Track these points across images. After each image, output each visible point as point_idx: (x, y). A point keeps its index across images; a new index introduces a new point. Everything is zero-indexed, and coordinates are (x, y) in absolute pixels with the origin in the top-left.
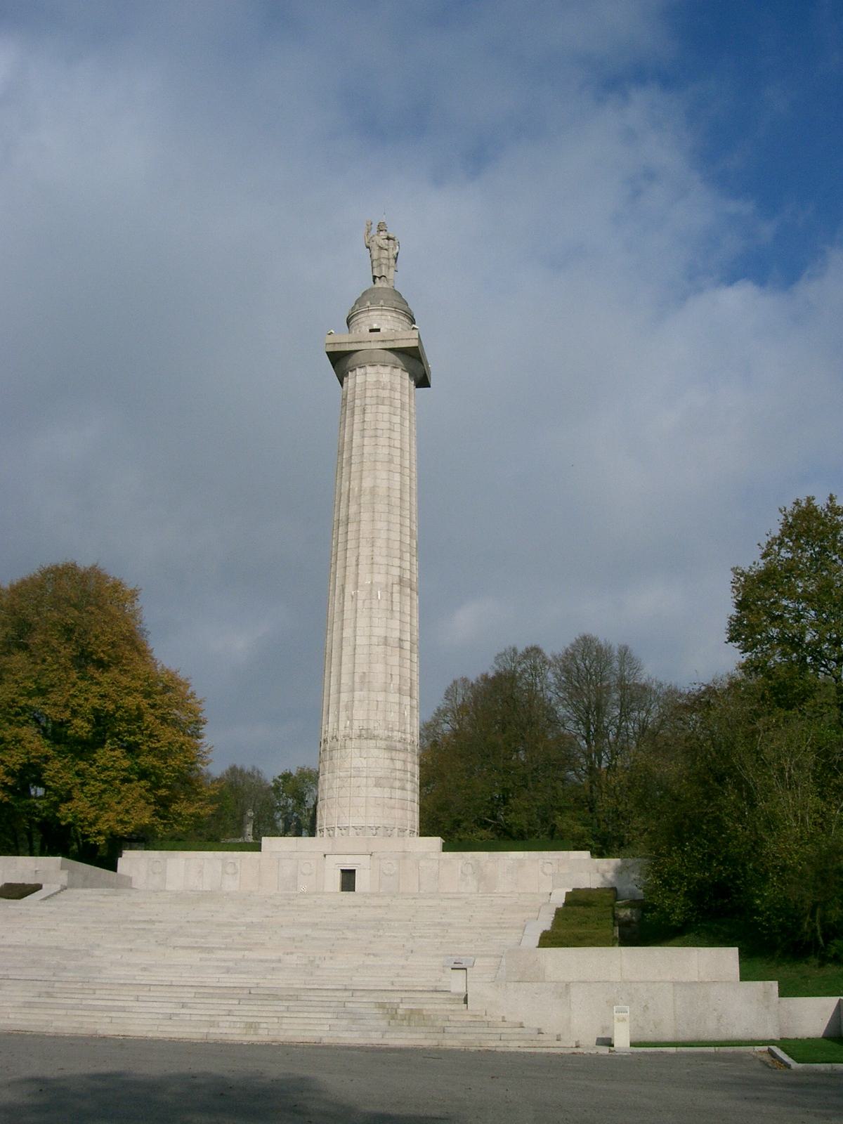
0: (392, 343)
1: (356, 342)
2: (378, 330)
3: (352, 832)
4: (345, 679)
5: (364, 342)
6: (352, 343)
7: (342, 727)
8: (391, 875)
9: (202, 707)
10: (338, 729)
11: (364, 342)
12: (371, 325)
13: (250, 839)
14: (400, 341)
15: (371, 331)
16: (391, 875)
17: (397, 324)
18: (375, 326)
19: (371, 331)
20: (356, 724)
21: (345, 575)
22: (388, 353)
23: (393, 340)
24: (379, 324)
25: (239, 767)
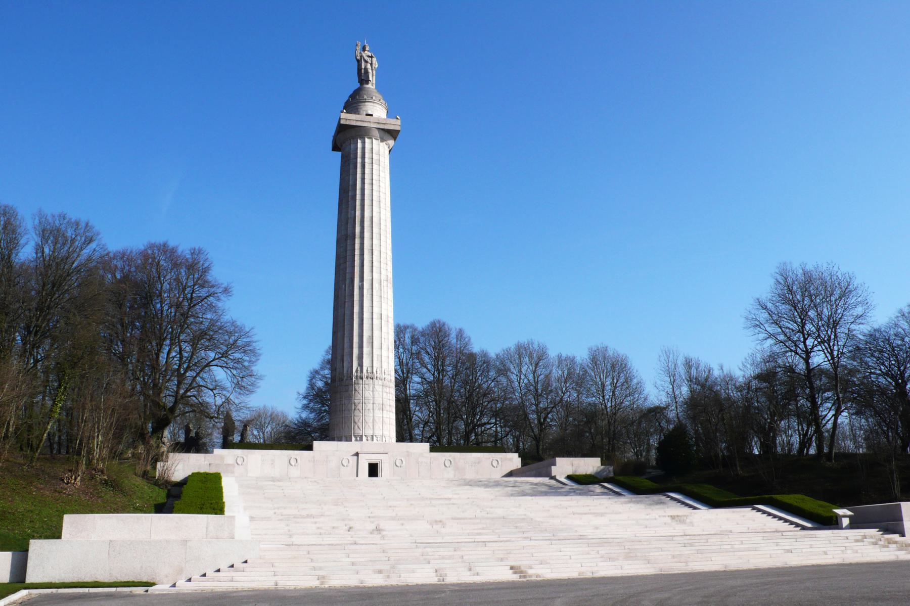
15: (367, 115)
18: (370, 112)
19: (367, 115)
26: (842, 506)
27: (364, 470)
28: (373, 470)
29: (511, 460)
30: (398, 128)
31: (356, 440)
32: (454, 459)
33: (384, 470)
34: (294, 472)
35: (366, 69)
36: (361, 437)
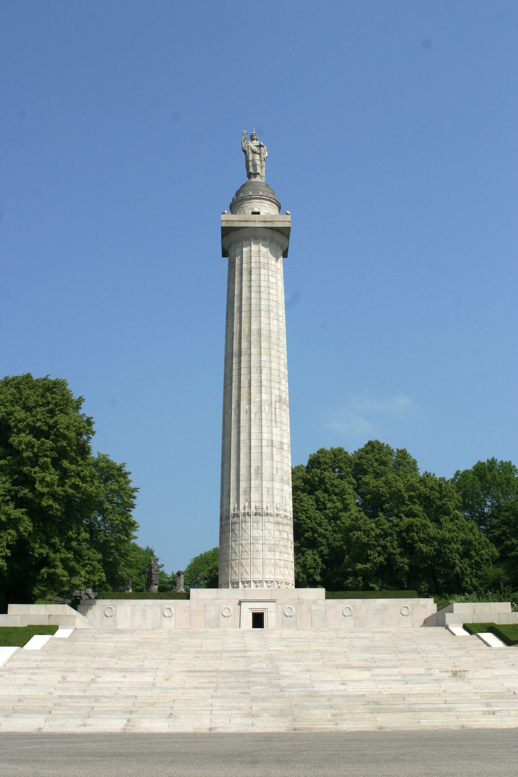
0: (271, 223)
1: (245, 221)
2: (258, 213)
3: (253, 584)
4: (243, 471)
5: (250, 221)
6: (240, 221)
7: (241, 507)
8: (290, 617)
9: (135, 494)
10: (238, 508)
11: (250, 221)
12: (253, 209)
13: (182, 590)
14: (278, 223)
15: (254, 213)
16: (290, 617)
17: (271, 210)
18: (256, 210)
19: (254, 213)
20: (253, 505)
21: (250, 393)
22: (268, 231)
23: (272, 222)
24: (259, 209)
25: (512, 465)
26: (351, 571)
27: (248, 620)
28: (258, 620)
29: (425, 606)
30: (287, 225)
31: (234, 587)
32: (354, 606)
33: (269, 620)
34: (169, 624)
35: (253, 160)
36: (237, 583)
